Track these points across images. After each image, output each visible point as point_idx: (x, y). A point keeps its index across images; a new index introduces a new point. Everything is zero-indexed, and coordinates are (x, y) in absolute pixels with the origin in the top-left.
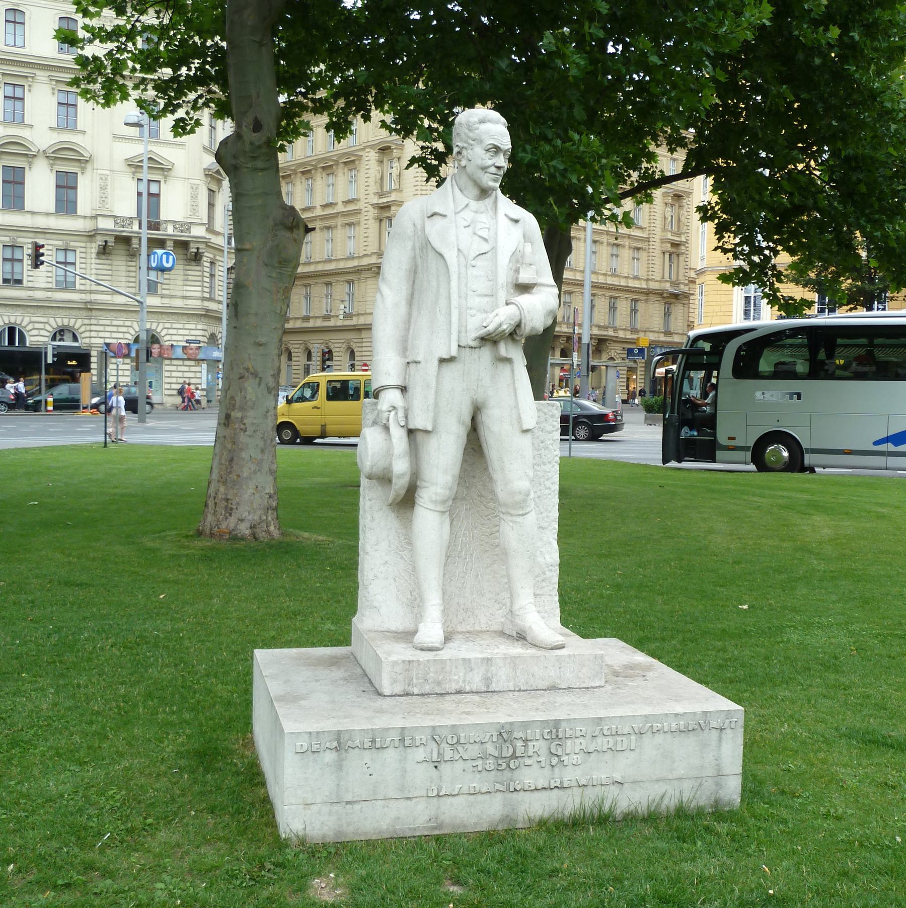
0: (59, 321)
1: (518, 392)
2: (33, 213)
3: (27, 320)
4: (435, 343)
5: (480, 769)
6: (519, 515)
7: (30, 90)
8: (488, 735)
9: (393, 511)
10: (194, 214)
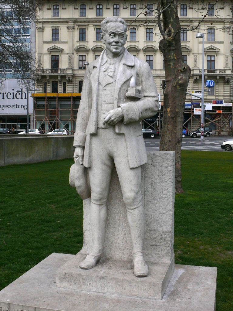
4: (91, 129)
7: (138, 30)
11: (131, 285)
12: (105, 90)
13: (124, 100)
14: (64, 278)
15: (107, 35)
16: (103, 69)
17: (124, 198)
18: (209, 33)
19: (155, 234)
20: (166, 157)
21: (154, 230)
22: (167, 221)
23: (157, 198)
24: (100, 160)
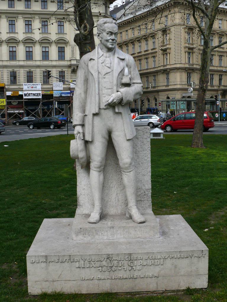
2: (52, 61)
4: (92, 108)
5: (101, 271)
11: (136, 230)
12: (104, 78)
13: (120, 86)
14: (79, 233)
16: (101, 60)
18: (59, 25)
19: (140, 191)
20: (145, 130)
22: (148, 181)
23: (140, 163)
24: (101, 135)
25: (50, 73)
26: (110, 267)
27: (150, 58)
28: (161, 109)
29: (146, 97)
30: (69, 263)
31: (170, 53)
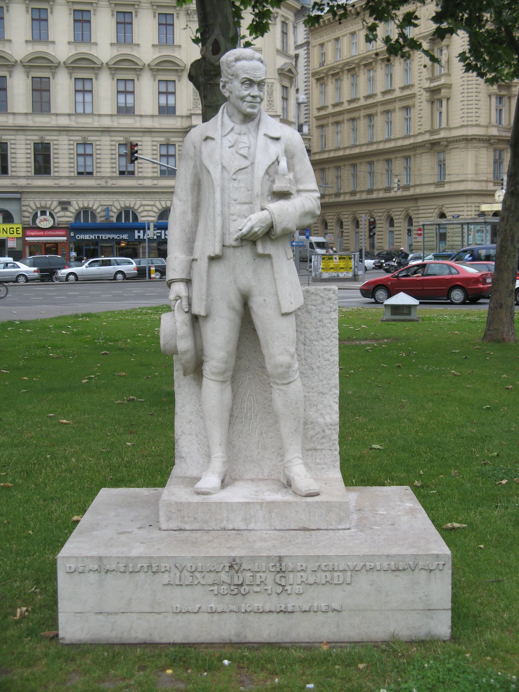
0: (163, 203)
1: (277, 281)
2: (141, 116)
3: (138, 203)
4: (208, 245)
6: (283, 384)
8: (222, 566)
9: (195, 380)
10: (270, 108)
12: (235, 180)
13: (269, 198)
15: (236, 84)
17: (269, 367)
19: (313, 429)
20: (327, 295)
21: (312, 423)
25: (136, 149)
26: (235, 585)
27: (379, 114)
28: (421, 244)
29: (437, 211)
30: (148, 574)
31: (448, 99)
